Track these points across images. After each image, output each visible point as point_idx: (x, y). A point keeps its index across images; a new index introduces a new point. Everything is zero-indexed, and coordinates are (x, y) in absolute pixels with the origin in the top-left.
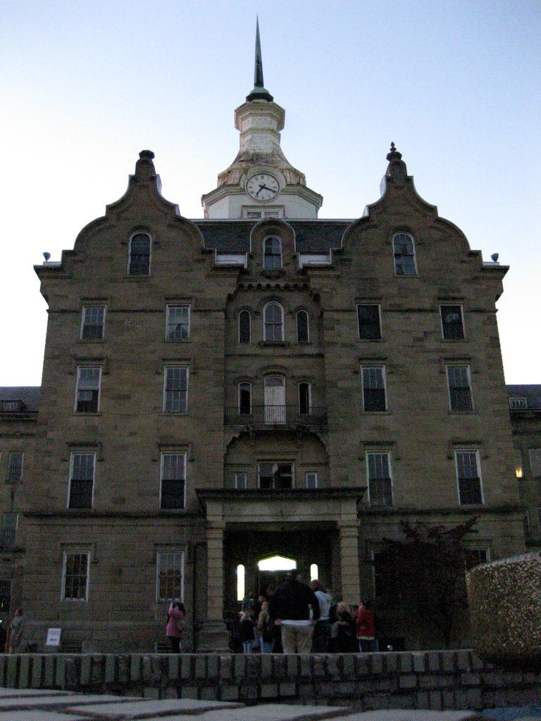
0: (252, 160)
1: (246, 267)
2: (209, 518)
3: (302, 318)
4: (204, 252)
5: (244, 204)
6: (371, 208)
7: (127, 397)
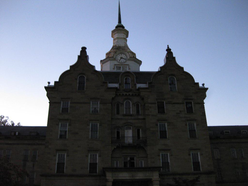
0: (118, 48)
1: (118, 88)
2: (107, 178)
3: (138, 106)
4: (104, 83)
5: (115, 64)
6: (161, 68)
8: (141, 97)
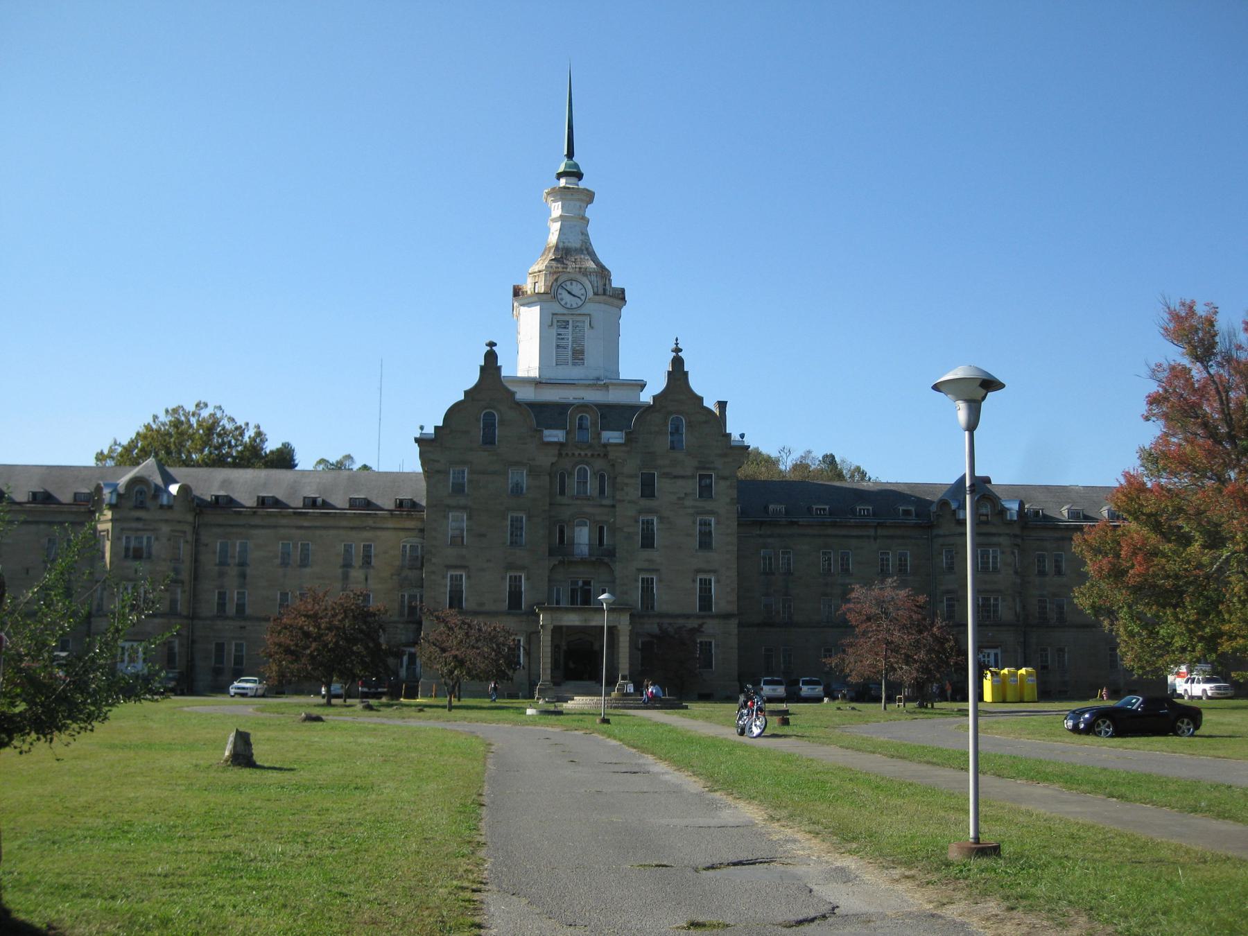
3: (602, 477)
7: (484, 535)
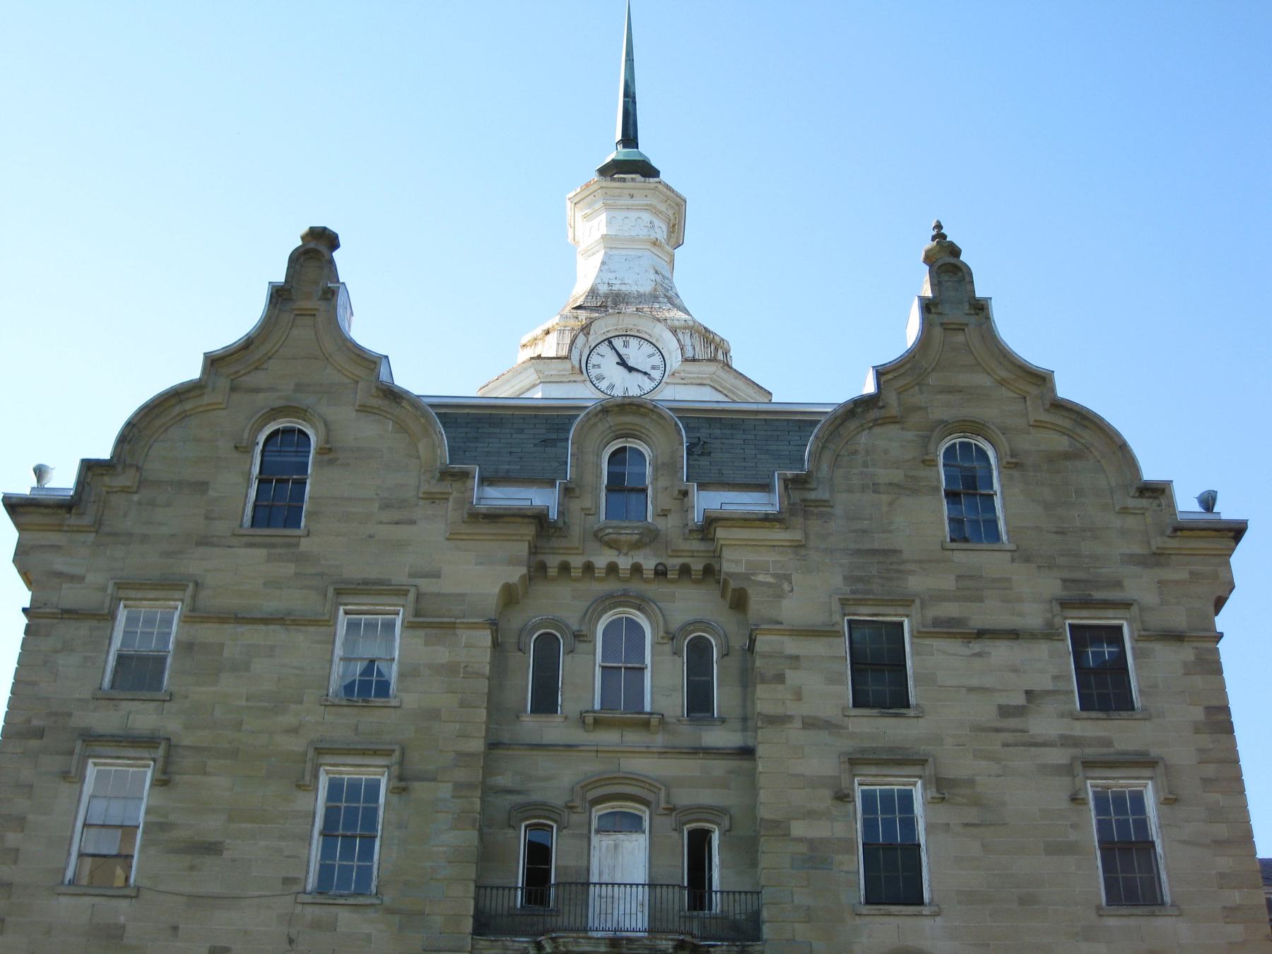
1: (553, 515)
4: (446, 475)
7: (212, 848)
8: (726, 581)
